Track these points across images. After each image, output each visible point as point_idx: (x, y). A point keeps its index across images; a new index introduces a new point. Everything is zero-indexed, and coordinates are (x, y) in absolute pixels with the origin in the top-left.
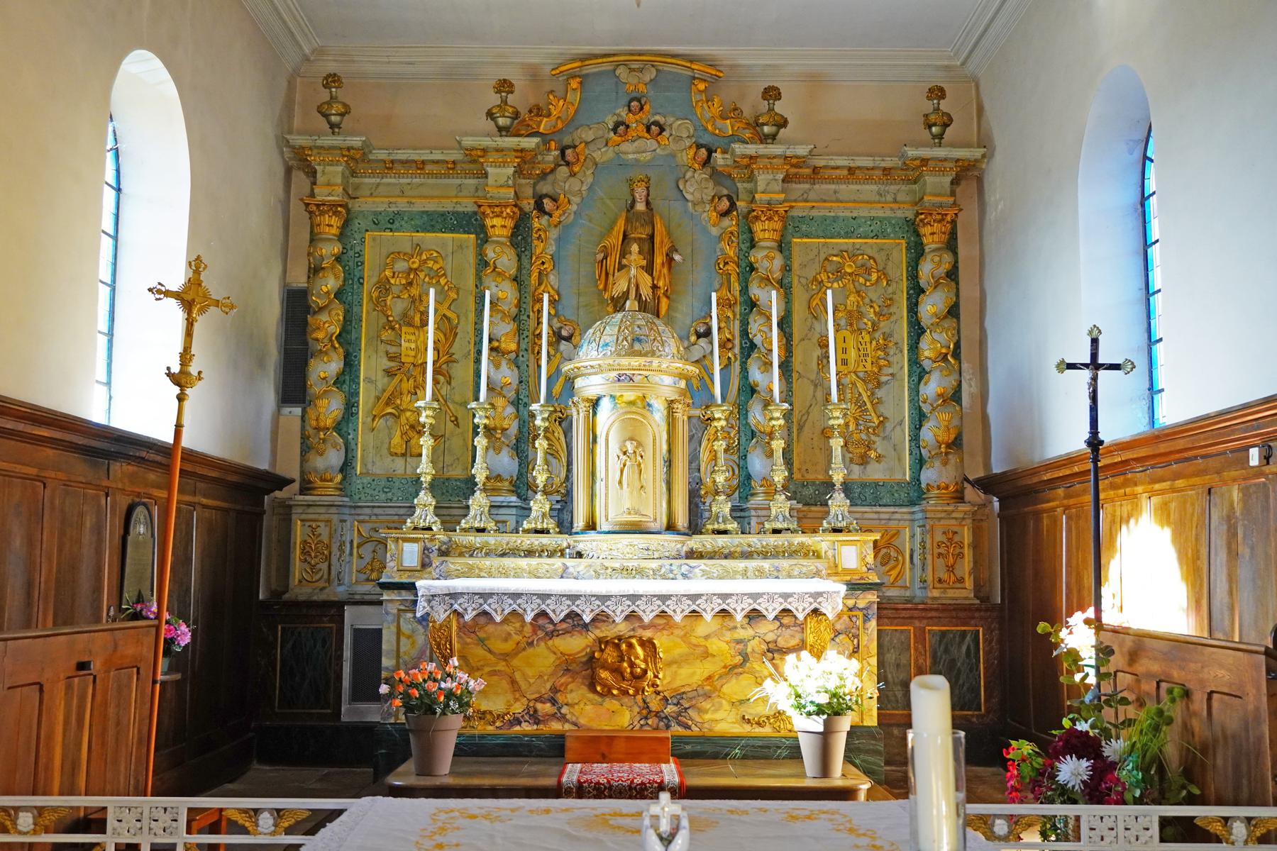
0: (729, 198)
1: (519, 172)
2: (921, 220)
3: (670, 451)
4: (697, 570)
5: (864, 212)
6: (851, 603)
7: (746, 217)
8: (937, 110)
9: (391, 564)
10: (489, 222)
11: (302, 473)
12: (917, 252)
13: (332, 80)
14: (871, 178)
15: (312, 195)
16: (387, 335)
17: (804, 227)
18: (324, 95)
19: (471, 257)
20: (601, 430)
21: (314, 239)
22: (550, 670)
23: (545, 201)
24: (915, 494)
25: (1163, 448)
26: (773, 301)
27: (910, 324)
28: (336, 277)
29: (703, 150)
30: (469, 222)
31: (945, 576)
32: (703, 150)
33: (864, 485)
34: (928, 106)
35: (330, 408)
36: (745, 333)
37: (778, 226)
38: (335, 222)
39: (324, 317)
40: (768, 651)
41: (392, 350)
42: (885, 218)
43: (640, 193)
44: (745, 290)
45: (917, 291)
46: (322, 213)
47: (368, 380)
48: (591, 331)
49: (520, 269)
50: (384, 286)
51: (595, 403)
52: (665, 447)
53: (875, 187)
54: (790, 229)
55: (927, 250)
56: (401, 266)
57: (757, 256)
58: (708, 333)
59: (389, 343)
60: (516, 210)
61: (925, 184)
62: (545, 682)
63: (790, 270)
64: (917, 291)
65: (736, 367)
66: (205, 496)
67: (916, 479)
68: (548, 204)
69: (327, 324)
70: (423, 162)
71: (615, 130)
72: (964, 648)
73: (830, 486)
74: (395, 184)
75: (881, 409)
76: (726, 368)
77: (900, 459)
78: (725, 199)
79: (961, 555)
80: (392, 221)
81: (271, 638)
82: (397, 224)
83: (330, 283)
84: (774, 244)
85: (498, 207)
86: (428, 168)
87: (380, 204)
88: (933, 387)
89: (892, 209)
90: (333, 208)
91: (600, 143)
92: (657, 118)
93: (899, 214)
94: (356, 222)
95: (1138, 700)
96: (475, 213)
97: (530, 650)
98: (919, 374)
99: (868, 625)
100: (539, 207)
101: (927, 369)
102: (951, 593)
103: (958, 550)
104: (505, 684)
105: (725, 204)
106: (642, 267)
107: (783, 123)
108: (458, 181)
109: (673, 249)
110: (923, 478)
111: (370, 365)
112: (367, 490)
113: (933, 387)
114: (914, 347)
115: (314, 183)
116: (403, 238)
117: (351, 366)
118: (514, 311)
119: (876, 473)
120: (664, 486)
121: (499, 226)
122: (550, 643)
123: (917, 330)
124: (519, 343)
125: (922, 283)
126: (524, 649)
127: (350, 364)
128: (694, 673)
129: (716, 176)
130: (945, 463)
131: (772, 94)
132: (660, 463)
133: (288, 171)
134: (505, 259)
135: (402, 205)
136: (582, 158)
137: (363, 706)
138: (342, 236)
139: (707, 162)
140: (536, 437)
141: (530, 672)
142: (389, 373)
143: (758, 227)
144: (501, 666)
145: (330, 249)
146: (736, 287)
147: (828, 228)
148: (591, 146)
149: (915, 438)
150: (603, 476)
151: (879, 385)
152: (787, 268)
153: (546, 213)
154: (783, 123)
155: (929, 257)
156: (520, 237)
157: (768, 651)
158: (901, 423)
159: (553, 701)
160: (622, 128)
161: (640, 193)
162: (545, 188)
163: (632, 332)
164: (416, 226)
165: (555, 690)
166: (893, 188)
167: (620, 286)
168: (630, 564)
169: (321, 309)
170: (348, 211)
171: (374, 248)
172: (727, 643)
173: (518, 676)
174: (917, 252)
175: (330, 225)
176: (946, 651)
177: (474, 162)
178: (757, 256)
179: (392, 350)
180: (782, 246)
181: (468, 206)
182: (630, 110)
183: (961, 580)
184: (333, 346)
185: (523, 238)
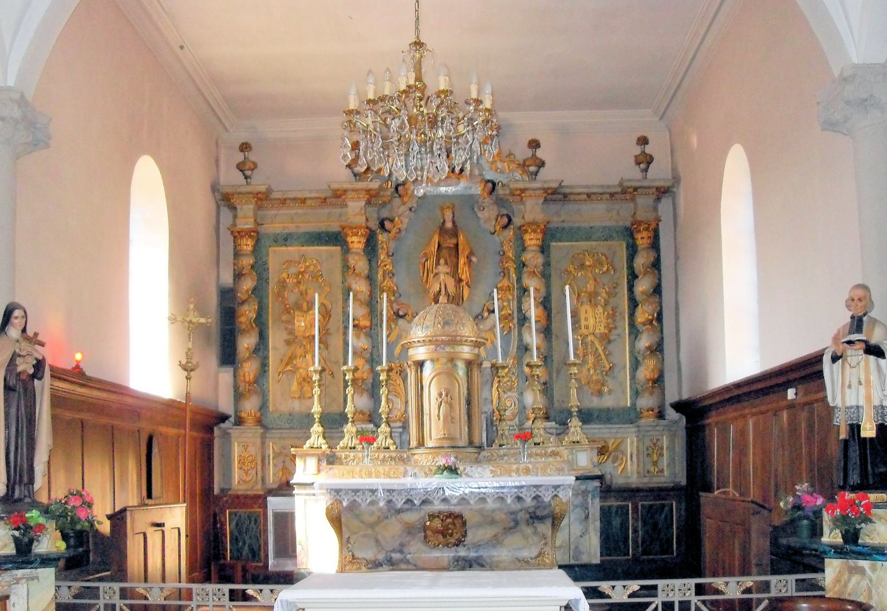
1: (368, 203)
6: (583, 487)
10: (349, 239)
11: (236, 412)
12: (632, 251)
13: (245, 147)
15: (234, 225)
16: (284, 318)
18: (240, 157)
19: (338, 261)
20: (426, 383)
21: (237, 254)
24: (630, 416)
25: (755, 387)
26: (533, 284)
30: (336, 239)
33: (600, 410)
34: (638, 150)
35: (249, 369)
36: (520, 310)
37: (540, 236)
38: (250, 242)
39: (246, 308)
44: (519, 280)
45: (633, 276)
46: (242, 237)
47: (275, 348)
49: (370, 270)
50: (283, 284)
51: (420, 364)
54: (549, 235)
56: (293, 270)
57: (527, 257)
58: (493, 311)
59: (288, 322)
64: (633, 276)
65: (515, 333)
67: (634, 405)
68: (387, 224)
69: (247, 313)
72: (663, 516)
73: (570, 414)
75: (611, 358)
76: (506, 339)
77: (624, 392)
79: (661, 455)
80: (286, 239)
83: (248, 284)
85: (354, 228)
86: (309, 202)
88: (645, 341)
90: (248, 233)
97: (386, 521)
98: (635, 332)
100: (382, 225)
102: (655, 480)
104: (372, 542)
107: (542, 164)
109: (472, 253)
111: (276, 338)
114: (632, 315)
115: (235, 217)
116: (293, 251)
119: (608, 402)
121: (357, 242)
122: (398, 516)
123: (634, 304)
127: (263, 337)
131: (534, 144)
132: (463, 402)
133: (218, 207)
134: (360, 263)
135: (292, 228)
137: (282, 561)
138: (256, 250)
142: (288, 343)
143: (527, 237)
144: (369, 531)
145: (247, 261)
146: (514, 276)
147: (572, 234)
149: (633, 378)
151: (609, 342)
152: (547, 264)
153: (386, 231)
154: (542, 164)
159: (401, 552)
162: (385, 213)
165: (402, 545)
166: (617, 206)
171: (276, 257)
173: (379, 537)
174: (632, 251)
175: (247, 245)
176: (652, 517)
177: (338, 196)
178: (527, 257)
179: (290, 327)
180: (544, 249)
181: (335, 227)
183: (662, 471)
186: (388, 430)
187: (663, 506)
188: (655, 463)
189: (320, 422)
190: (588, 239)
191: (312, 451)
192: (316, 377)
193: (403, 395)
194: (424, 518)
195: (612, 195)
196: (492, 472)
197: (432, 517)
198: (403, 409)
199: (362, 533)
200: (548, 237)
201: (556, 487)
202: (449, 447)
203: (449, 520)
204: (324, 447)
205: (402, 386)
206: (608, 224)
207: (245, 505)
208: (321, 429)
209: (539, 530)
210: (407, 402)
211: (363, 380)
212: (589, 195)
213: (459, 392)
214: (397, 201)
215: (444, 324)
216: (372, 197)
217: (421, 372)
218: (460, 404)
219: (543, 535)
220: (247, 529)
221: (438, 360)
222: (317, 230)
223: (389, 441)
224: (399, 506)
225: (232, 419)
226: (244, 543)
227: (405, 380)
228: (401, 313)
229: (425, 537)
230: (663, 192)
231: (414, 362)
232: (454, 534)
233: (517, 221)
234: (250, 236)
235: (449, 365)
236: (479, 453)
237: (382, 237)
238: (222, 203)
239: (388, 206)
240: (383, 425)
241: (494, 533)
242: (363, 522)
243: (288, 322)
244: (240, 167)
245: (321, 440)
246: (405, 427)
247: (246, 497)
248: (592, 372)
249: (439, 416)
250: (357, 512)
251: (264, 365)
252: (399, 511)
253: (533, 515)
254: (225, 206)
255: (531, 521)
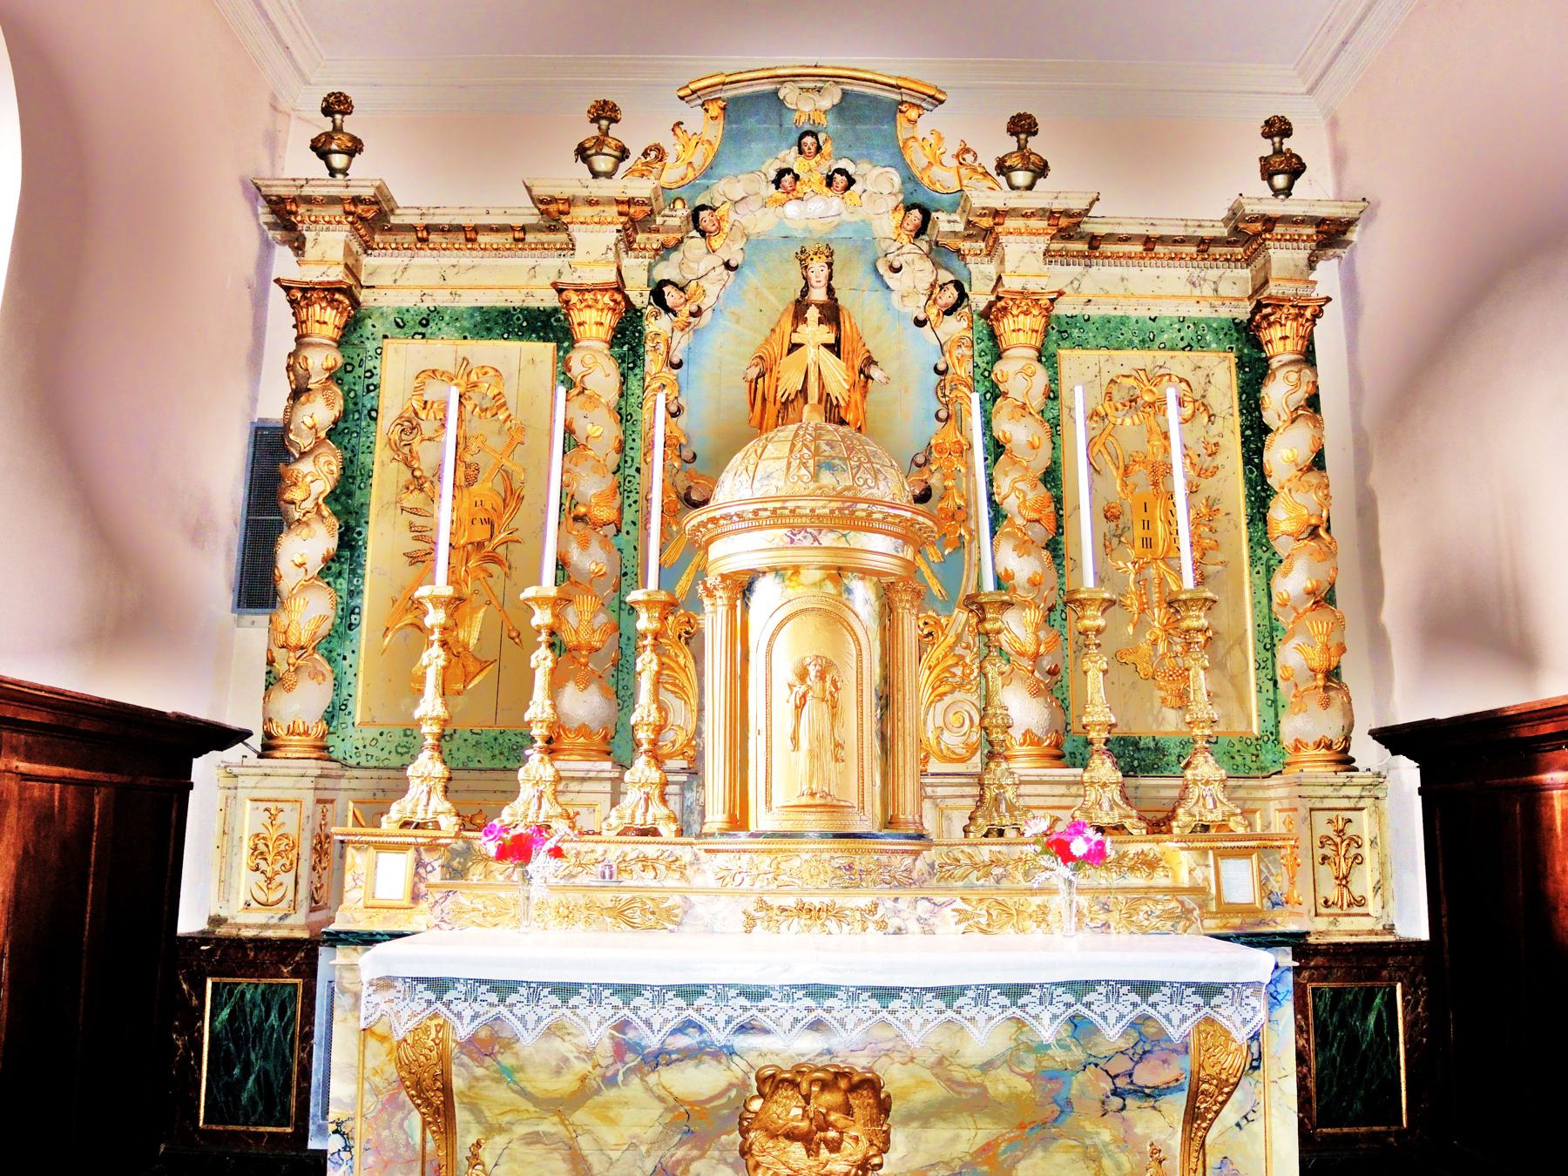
0: (958, 285)
2: (1266, 317)
3: (886, 679)
4: (947, 911)
5: (1168, 311)
7: (985, 315)
8: (1278, 152)
9: (353, 894)
12: (1254, 373)
14: (1178, 257)
16: (414, 500)
17: (1075, 333)
18: (326, 124)
22: (651, 1134)
23: (666, 289)
27: (1250, 483)
28: (330, 404)
29: (916, 213)
30: (546, 326)
31: (1333, 895)
32: (916, 213)
34: (1266, 148)
35: (307, 610)
37: (1039, 323)
39: (304, 467)
40: (1115, 1093)
41: (419, 521)
42: (1202, 320)
43: (818, 270)
48: (739, 456)
51: (743, 586)
52: (877, 670)
53: (1183, 273)
55: (1274, 363)
57: (1006, 370)
59: (414, 511)
60: (618, 297)
61: (1268, 261)
62: (642, 1158)
63: (1056, 398)
66: (29, 758)
69: (313, 477)
70: (476, 229)
71: (777, 183)
72: (1372, 1020)
74: (430, 267)
77: (1242, 700)
78: (951, 286)
80: (424, 323)
81: (195, 1002)
82: (433, 326)
83: (320, 412)
84: (1034, 353)
87: (407, 299)
88: (1294, 582)
89: (1212, 306)
90: (330, 291)
91: (754, 203)
92: (842, 164)
93: (1225, 313)
94: (369, 322)
95: (461, 600)
96: (556, 310)
97: (610, 1094)
99: (1277, 1012)
100: (658, 295)
101: (1282, 553)
103: (1353, 851)
105: (951, 295)
106: (826, 346)
108: (531, 262)
110: (1283, 728)
112: (369, 750)
113: (1294, 582)
116: (443, 350)
117: (352, 548)
118: (614, 459)
120: (877, 743)
121: (593, 323)
122: (652, 1079)
124: (621, 510)
125: (1269, 417)
126: (598, 1091)
127: (349, 543)
128: (955, 1139)
129: (939, 253)
130: (1326, 704)
132: (870, 699)
133: (267, 245)
135: (441, 299)
136: (726, 227)
139: (921, 231)
140: (637, 650)
141: (610, 1135)
144: (549, 1125)
145: (320, 360)
147: (1113, 333)
148: (740, 207)
150: (762, 726)
153: (668, 310)
155: (1280, 374)
156: (627, 337)
157: (1115, 1093)
158: (1241, 641)
160: (788, 178)
161: (818, 270)
162: (664, 271)
163: (817, 452)
164: (463, 329)
166: (1213, 274)
167: (790, 381)
168: (816, 902)
169: (303, 455)
170: (355, 303)
171: (399, 367)
172: (1028, 1077)
173: (584, 1143)
174: (1254, 373)
175: (326, 320)
176: (1343, 1024)
179: (419, 521)
180: (1045, 357)
182: (801, 152)
183: (1361, 902)
184: (319, 512)
185: (631, 349)
186: (655, 775)
187: (1370, 995)
188: (1343, 881)
189: (438, 748)
190: (1146, 343)
191: (410, 837)
192: (435, 618)
193: (692, 692)
194: (744, 1085)
195: (1204, 244)
196: (963, 916)
197: (771, 1083)
198: (691, 728)
199: (521, 1130)
200: (1054, 335)
201: (1208, 991)
202: (823, 835)
203: (831, 1098)
204: (449, 824)
205: (691, 665)
206: (1193, 311)
207: (256, 969)
208: (439, 770)
209: (1139, 1130)
210: (701, 709)
211: (593, 650)
212: (1149, 242)
213: (859, 672)
214: (695, 244)
215: (818, 466)
216: (636, 221)
217: (746, 606)
218: (860, 703)
219: (1155, 1151)
220: (259, 1030)
221: (796, 570)
222: (501, 304)
223: (657, 810)
224: (653, 1042)
225: (256, 741)
226: (246, 1073)
227: (698, 658)
228: (695, 497)
229: (745, 1152)
230: (1331, 234)
231: (724, 577)
232: (847, 1145)
233: (980, 297)
234: (331, 302)
235: (830, 588)
236: (917, 853)
237: (657, 325)
238: (278, 234)
239: (675, 257)
240: (641, 762)
241: (982, 1138)
242: (524, 1093)
243: (414, 511)
244: (321, 148)
245: (439, 803)
246: (694, 772)
247: (260, 944)
248: (1162, 647)
249: (795, 739)
250: (507, 1060)
251: (348, 617)
252: (657, 1059)
253: (1122, 1083)
254: (284, 243)
255: (1116, 1102)
